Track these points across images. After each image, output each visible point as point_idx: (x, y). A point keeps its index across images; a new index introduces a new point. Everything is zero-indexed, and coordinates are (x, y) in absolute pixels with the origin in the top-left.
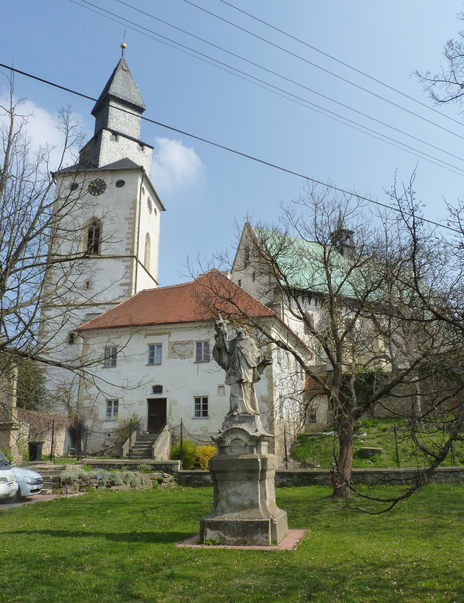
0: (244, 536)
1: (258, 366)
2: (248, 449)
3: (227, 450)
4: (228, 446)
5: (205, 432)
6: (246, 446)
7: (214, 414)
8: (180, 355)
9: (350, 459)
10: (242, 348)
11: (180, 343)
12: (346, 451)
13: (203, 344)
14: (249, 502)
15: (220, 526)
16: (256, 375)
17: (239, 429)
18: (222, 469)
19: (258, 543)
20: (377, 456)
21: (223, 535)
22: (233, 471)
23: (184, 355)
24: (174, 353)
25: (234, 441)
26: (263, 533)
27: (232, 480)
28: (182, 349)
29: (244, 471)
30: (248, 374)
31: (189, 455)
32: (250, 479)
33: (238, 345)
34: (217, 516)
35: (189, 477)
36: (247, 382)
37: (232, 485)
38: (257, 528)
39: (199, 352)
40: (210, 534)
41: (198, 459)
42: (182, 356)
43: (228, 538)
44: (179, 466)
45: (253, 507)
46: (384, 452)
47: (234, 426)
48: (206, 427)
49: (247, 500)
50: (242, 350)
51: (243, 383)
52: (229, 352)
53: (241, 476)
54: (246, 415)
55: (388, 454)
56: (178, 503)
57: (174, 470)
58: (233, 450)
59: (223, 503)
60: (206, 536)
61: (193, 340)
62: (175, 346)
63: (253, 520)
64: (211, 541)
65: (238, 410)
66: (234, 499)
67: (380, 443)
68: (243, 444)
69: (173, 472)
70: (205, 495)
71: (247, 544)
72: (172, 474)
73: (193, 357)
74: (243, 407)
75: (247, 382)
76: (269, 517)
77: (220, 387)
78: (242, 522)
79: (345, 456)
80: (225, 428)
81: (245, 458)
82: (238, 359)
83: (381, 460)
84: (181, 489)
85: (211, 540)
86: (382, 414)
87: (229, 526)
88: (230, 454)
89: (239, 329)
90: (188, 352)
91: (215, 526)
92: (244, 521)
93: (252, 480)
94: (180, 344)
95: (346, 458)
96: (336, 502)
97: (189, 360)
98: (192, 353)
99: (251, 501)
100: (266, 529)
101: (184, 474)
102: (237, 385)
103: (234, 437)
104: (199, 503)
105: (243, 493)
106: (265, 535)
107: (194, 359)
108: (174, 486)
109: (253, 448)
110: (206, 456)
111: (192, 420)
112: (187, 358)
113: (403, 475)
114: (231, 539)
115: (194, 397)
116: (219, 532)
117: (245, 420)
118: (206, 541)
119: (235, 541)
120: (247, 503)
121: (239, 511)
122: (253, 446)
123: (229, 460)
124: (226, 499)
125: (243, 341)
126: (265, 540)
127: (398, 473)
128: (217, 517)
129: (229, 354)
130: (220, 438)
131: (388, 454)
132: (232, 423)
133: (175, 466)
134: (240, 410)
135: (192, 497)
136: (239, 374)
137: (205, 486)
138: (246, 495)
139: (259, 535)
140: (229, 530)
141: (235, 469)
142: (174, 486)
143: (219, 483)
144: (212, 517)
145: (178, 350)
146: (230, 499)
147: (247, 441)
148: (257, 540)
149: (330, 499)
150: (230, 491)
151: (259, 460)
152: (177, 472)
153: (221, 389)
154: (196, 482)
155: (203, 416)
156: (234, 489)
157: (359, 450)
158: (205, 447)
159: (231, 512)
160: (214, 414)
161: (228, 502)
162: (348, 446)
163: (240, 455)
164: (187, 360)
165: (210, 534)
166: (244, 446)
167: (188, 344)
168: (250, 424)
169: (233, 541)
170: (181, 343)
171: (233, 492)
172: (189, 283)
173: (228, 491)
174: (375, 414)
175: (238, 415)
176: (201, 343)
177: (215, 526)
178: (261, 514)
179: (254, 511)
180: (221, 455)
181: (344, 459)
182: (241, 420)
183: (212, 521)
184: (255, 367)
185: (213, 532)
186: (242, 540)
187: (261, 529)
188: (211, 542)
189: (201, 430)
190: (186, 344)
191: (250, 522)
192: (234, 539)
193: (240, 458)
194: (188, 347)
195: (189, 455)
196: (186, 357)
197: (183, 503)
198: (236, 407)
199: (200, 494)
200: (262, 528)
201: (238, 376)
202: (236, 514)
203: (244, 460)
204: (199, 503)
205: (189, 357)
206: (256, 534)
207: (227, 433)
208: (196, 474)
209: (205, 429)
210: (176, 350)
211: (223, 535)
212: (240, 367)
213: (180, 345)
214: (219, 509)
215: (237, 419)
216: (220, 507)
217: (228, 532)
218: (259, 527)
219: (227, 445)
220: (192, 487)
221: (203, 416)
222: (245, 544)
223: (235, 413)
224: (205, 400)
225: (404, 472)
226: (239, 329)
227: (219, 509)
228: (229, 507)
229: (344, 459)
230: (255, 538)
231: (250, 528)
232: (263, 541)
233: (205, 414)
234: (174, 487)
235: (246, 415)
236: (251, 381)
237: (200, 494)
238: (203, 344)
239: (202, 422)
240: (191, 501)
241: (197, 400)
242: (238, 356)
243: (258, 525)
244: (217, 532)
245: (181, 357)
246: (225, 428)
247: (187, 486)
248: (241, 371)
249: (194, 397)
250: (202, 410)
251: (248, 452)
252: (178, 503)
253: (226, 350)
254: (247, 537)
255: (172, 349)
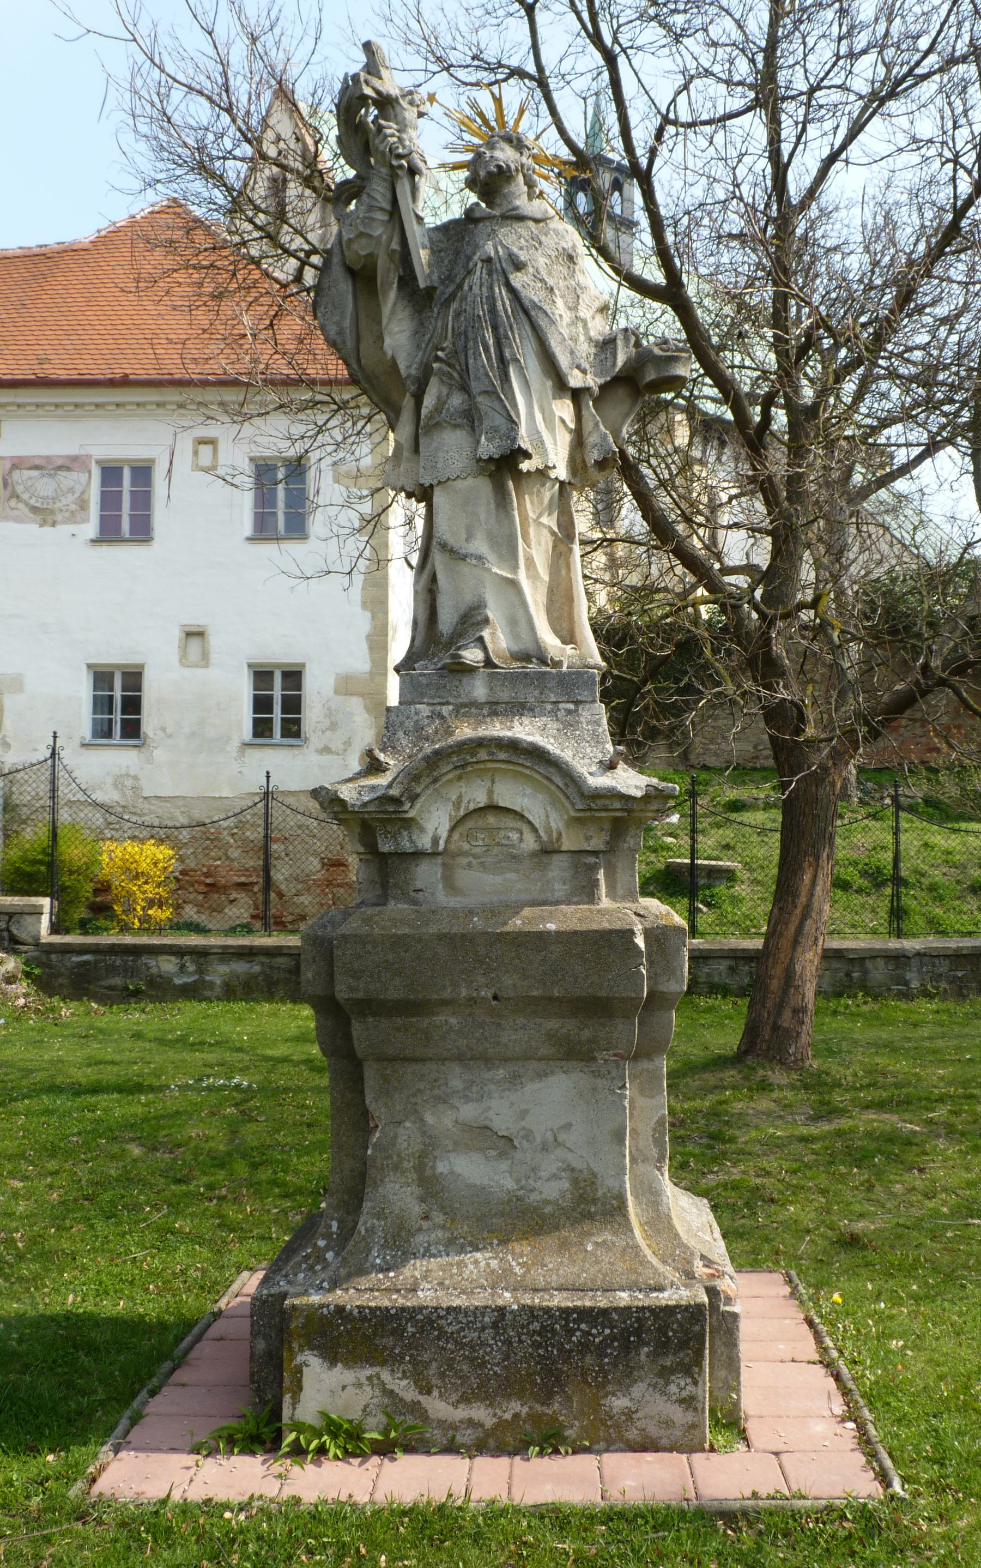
0: (547, 1399)
1: (602, 387)
2: (558, 869)
3: (426, 874)
4: (435, 854)
5: (129, 793)
6: (547, 851)
7: (163, 729)
8: (34, 510)
9: (820, 911)
10: (519, 266)
11: (37, 462)
12: (807, 878)
13: (127, 474)
14: (565, 1185)
15: (389, 1341)
16: (592, 439)
17: (513, 746)
18: (394, 991)
19: (632, 1434)
20: (720, 888)
21: (406, 1390)
22: (472, 1001)
23: (52, 512)
24: (13, 503)
25: (470, 824)
26: (665, 1374)
27: (460, 1058)
28: (46, 487)
29: (546, 1005)
30: (552, 430)
31: (71, 873)
32: (574, 1053)
33: (489, 248)
34: (362, 1271)
35: (86, 963)
36: (542, 474)
37: (456, 1084)
38: (627, 1348)
39: (110, 501)
40: (324, 1388)
41: (104, 888)
42: (44, 515)
43: (439, 1407)
44: (45, 920)
45: (590, 1216)
46: (743, 874)
47: (465, 731)
48: (136, 778)
49: (555, 1177)
50: (517, 280)
51: (519, 476)
52: (430, 291)
53: (516, 1033)
54: (533, 667)
55: (756, 882)
56: (54, 1089)
57: (22, 935)
58: (466, 877)
59: (398, 1194)
60: (295, 1402)
61: (89, 457)
62: (16, 475)
63: (602, 1302)
64: (333, 1428)
65: (486, 634)
66: (467, 1169)
67: (727, 847)
68: (530, 843)
69: (18, 942)
70: (161, 1041)
71: (564, 1440)
72: (16, 952)
73: (85, 520)
74: (519, 618)
75: (542, 474)
76: (690, 1275)
77: (189, 634)
78: (530, 1312)
79: (803, 899)
80: (403, 740)
81: (551, 926)
82: (495, 328)
83: (736, 901)
84: (52, 1010)
85: (331, 1422)
86: (716, 755)
87: (450, 1337)
88: (442, 898)
89: (498, 154)
90: (69, 501)
91: (357, 1338)
92: (547, 1310)
93: (588, 1058)
94: (36, 467)
95: (808, 908)
96: (765, 1087)
97: (71, 528)
98: (83, 505)
99: (575, 1182)
100: (686, 1356)
101: (67, 950)
102: (484, 487)
103: (476, 794)
104: (152, 1089)
105: (528, 1135)
106: (679, 1385)
107: (91, 528)
108: (26, 996)
109: (593, 868)
110: (137, 877)
111: (83, 750)
112: (66, 521)
113: (914, 962)
114: (462, 1413)
115: (89, 666)
116: (386, 1376)
117: (531, 696)
118: (299, 1427)
119: (489, 1422)
120: (553, 1190)
121: (504, 1242)
122: (595, 853)
123: (441, 937)
124: (420, 1169)
125: (520, 228)
126: (679, 1415)
127: (899, 959)
128: (363, 1283)
129: (420, 299)
130: (386, 799)
131: (756, 882)
132: (446, 710)
133: (29, 919)
134: (498, 639)
135: (109, 1053)
136: (499, 421)
137: (153, 999)
138: (544, 1148)
139: (638, 1390)
140: (451, 1363)
141: (486, 993)
142: (26, 996)
143: (370, 1073)
144: (335, 1284)
145: (27, 489)
146: (441, 1167)
147: (557, 822)
148: (629, 1414)
149: (731, 1075)
150: (441, 1120)
151: (640, 941)
152: (37, 944)
153: (195, 644)
154: (117, 981)
155: (124, 736)
156: (468, 1111)
157: (660, 866)
158: (132, 848)
159: (454, 1245)
160: (163, 729)
161: (431, 1188)
162: (817, 858)
163: (515, 909)
164: (64, 530)
165: (324, 1388)
166: (534, 854)
167: (69, 469)
168: (567, 725)
169: (471, 1423)
170: (41, 466)
171: (467, 1127)
172: (71, 244)
173: (430, 1119)
174: (692, 756)
175: (488, 663)
176: (120, 470)
177: (357, 1338)
178: (644, 1263)
179: (597, 1241)
180: (382, 900)
181: (798, 911)
182: (504, 695)
183: (340, 1310)
184: (588, 389)
185: (341, 1375)
186: (535, 1419)
187: (655, 1355)
188: (334, 1436)
189: (115, 785)
190: (60, 468)
191: (585, 1314)
192: (481, 1413)
193: (517, 923)
194: (68, 479)
195: (71, 873)
196: (59, 517)
197: (77, 1090)
198: (472, 621)
199: (138, 1036)
200: (663, 1347)
201: (496, 429)
202: (479, 1263)
203: (543, 936)
204: (152, 1089)
205: (72, 518)
206: (627, 1379)
207: (432, 768)
208: (114, 950)
209: (129, 783)
210: (19, 489)
211: (406, 1390)
212: (505, 378)
213: (35, 473)
214: (371, 1231)
215: (479, 689)
216: (380, 1216)
217: (442, 1375)
218: (641, 1343)
219: (425, 842)
220: (101, 1000)
221: (124, 736)
222: (550, 1441)
223: (472, 655)
224: (134, 678)
225: (918, 954)
226: (498, 154)
227: (371, 1231)
228: (438, 1218)
229: (798, 911)
230: (619, 1403)
231: (584, 1347)
232: (668, 1424)
233: (132, 730)
234: (22, 1001)
235: (533, 667)
236: (562, 472)
237: (138, 1036)
238: (127, 474)
239: (118, 759)
240: (109, 1075)
241: (102, 677)
242: (493, 311)
243: (638, 1332)
244: (369, 1372)
245: (39, 518)
246: (403, 740)
247: (79, 999)
248: (515, 406)
249: (89, 666)
250: (118, 716)
251: (560, 889)
252: (54, 1089)
253: (407, 279)
254: (569, 1399)
255: (5, 484)
